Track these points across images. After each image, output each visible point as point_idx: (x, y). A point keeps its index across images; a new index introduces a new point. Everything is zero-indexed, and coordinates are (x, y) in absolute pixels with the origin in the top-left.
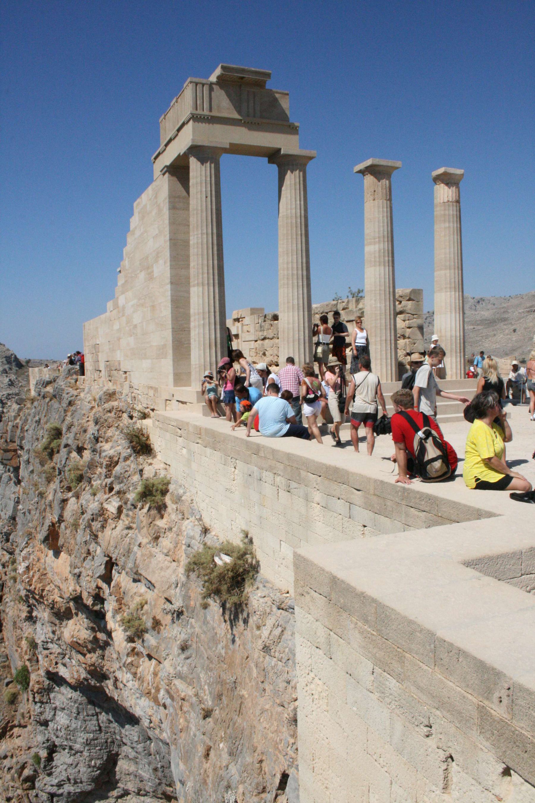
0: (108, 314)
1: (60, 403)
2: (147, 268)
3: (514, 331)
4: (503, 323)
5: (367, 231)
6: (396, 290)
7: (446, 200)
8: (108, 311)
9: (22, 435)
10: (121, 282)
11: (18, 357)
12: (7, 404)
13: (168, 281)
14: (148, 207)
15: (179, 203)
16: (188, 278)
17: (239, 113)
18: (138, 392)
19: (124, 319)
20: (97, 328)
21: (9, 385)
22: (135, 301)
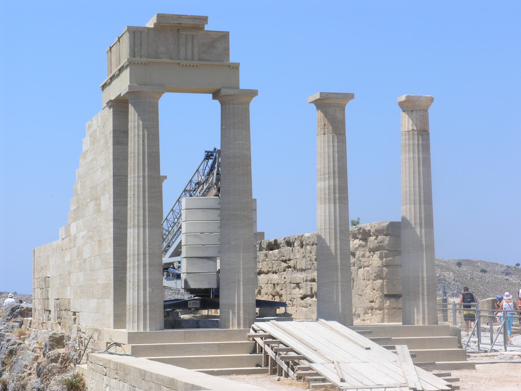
0: (60, 241)
19: (75, 250)
20: (48, 257)
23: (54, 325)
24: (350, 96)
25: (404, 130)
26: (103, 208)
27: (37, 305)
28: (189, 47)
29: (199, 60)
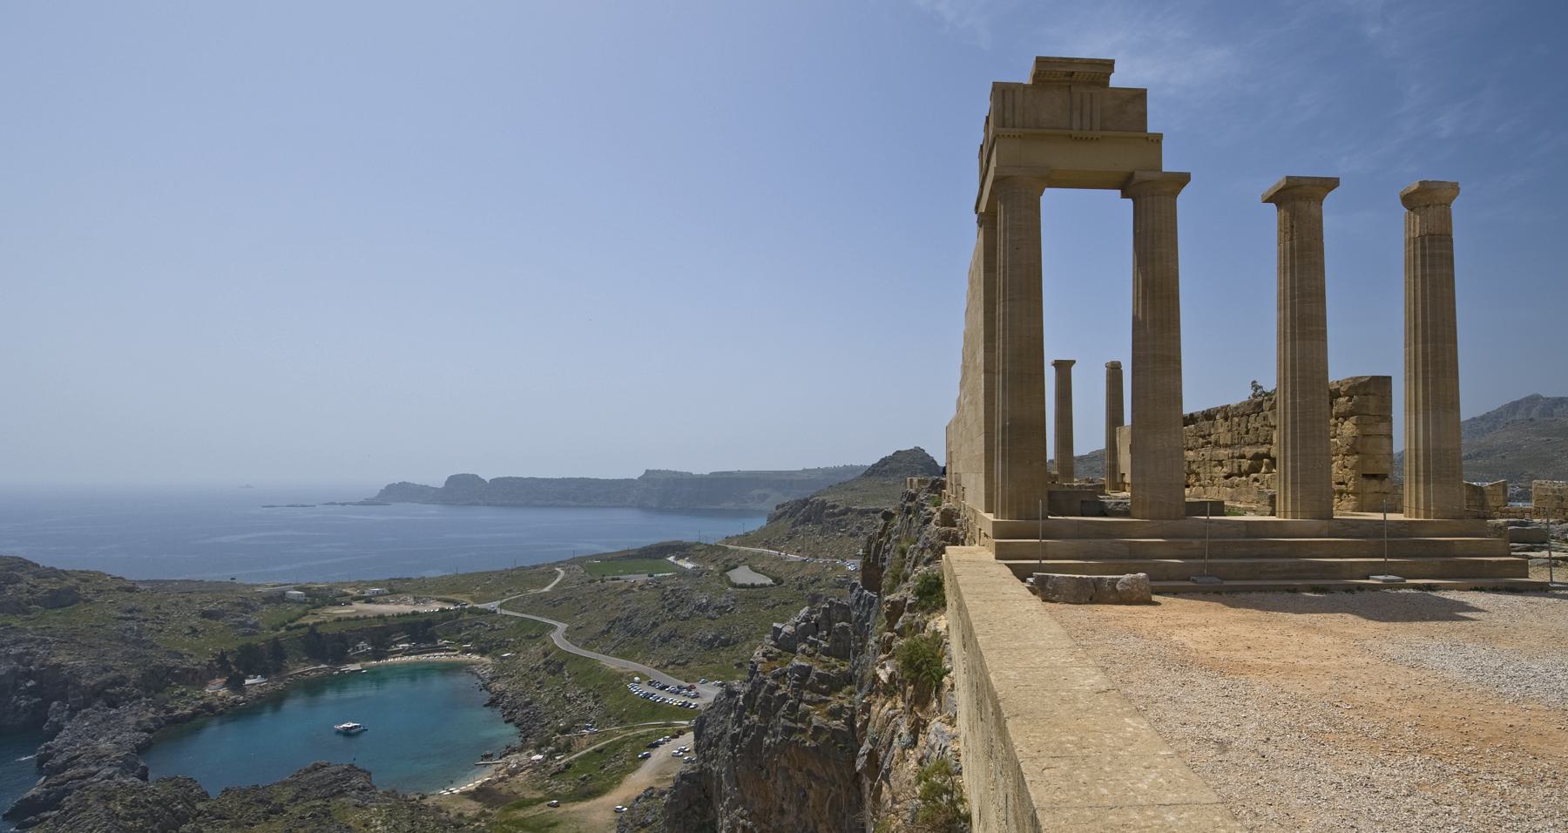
24: (1331, 184)
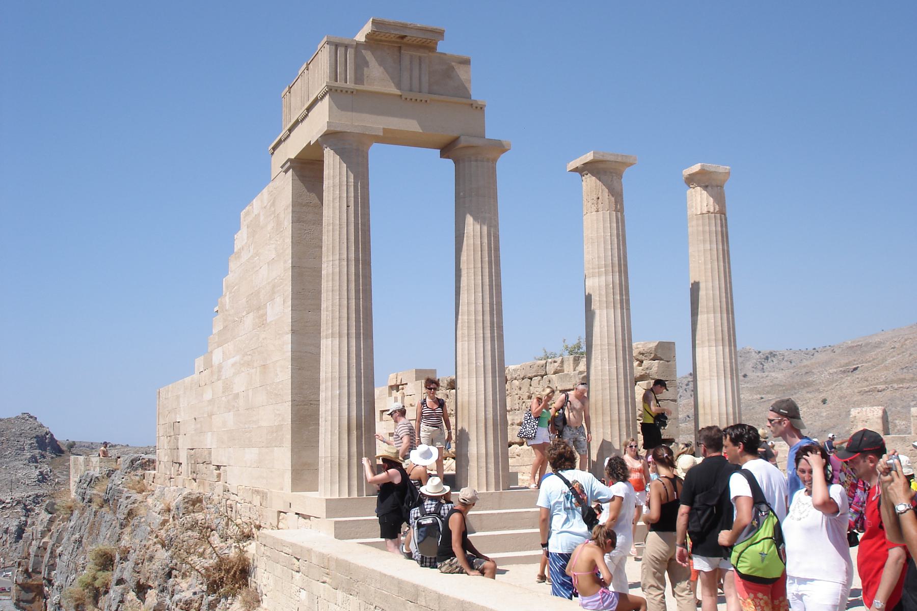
0: (196, 376)
1: (115, 513)
2: (258, 308)
3: (824, 401)
4: (807, 389)
5: (587, 257)
6: (634, 345)
7: (705, 210)
8: (197, 372)
9: (52, 562)
10: (217, 328)
11: (56, 437)
12: (33, 510)
13: (288, 328)
14: (262, 218)
15: (307, 214)
16: (318, 324)
17: (399, 86)
18: (237, 498)
19: (220, 384)
20: (178, 397)
21: (39, 481)
22: (237, 358)
23: (187, 482)
25: (695, 212)
26: (269, 319)
27: (162, 456)
28: (416, 73)
29: (429, 93)
